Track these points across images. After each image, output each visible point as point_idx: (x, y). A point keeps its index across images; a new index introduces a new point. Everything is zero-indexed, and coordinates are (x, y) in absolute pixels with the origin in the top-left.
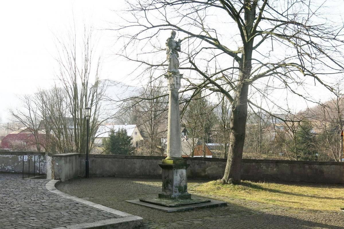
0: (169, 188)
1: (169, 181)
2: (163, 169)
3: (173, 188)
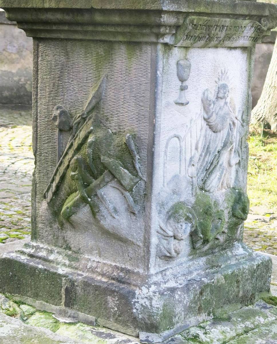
0: (107, 223)
1: (105, 159)
2: (38, 40)
3: (147, 231)
